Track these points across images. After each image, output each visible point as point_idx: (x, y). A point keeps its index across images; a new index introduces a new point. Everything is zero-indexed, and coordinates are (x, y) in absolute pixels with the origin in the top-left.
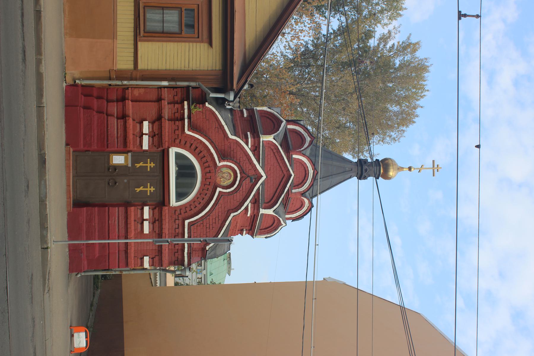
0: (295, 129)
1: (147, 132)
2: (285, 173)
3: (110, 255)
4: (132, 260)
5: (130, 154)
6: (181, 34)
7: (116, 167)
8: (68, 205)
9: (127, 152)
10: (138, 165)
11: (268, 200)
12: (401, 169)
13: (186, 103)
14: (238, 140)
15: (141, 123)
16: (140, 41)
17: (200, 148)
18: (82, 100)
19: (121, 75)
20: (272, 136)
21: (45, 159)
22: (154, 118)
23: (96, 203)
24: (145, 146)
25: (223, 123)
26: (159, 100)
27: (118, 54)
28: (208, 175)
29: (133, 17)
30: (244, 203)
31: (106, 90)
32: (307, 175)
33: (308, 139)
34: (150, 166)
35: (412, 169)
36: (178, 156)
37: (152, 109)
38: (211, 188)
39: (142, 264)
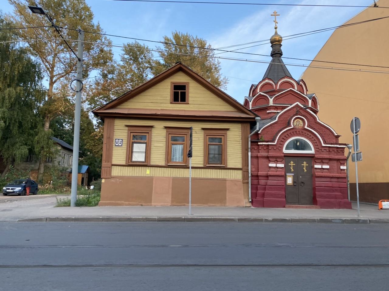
0: (260, 88)
1: (275, 164)
2: (288, 93)
3: (340, 187)
4: (342, 175)
5: (287, 174)
6: (222, 145)
7: (294, 182)
8: (316, 208)
9: (286, 175)
10: (292, 170)
11: (304, 102)
12: (276, 33)
13: (259, 143)
14: (278, 116)
15: (270, 167)
16: (227, 167)
17: (283, 136)
18: (258, 198)
19: (245, 177)
20: (250, 102)
21: (320, 219)
22: (268, 161)
23: (312, 193)
24: (283, 166)
25: (269, 124)
26: (257, 157)
27: (234, 178)
28: (298, 133)
29: (214, 170)
30: (312, 114)
31: (252, 186)
32: (288, 82)
33: (267, 81)
34: (293, 163)
35: (276, 27)
36: (287, 148)
37: (262, 161)
38: (304, 131)
39: (344, 170)
